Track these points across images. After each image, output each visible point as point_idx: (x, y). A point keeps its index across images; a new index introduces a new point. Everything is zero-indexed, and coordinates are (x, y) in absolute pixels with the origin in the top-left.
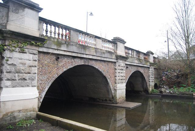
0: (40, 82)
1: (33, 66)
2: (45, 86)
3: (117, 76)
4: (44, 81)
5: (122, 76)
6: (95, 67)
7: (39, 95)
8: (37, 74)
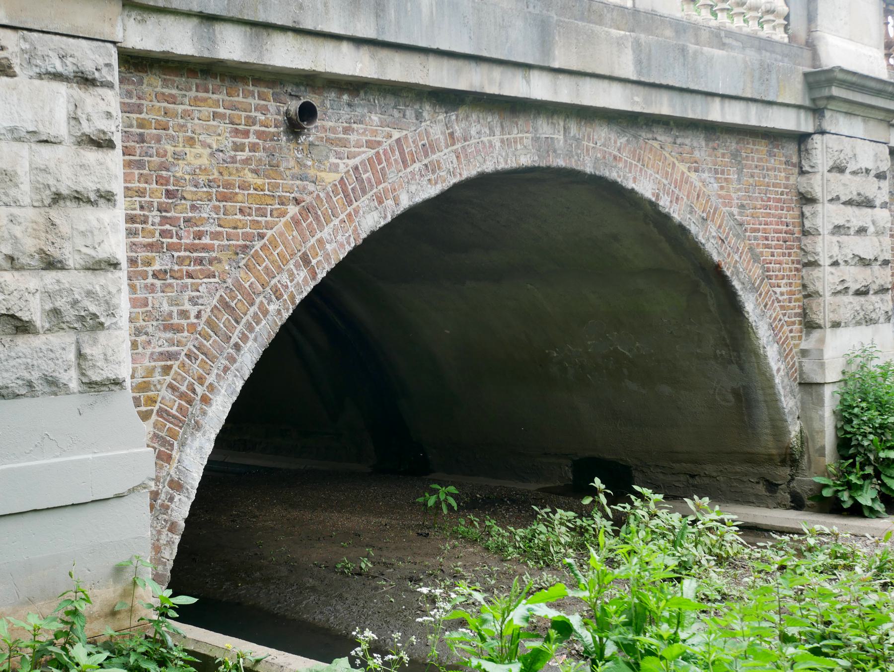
0: (161, 342)
1: (79, 198)
2: (201, 380)
3: (825, 261)
4: (192, 328)
5: (864, 262)
6: (630, 185)
7: (158, 467)
8: (122, 275)
